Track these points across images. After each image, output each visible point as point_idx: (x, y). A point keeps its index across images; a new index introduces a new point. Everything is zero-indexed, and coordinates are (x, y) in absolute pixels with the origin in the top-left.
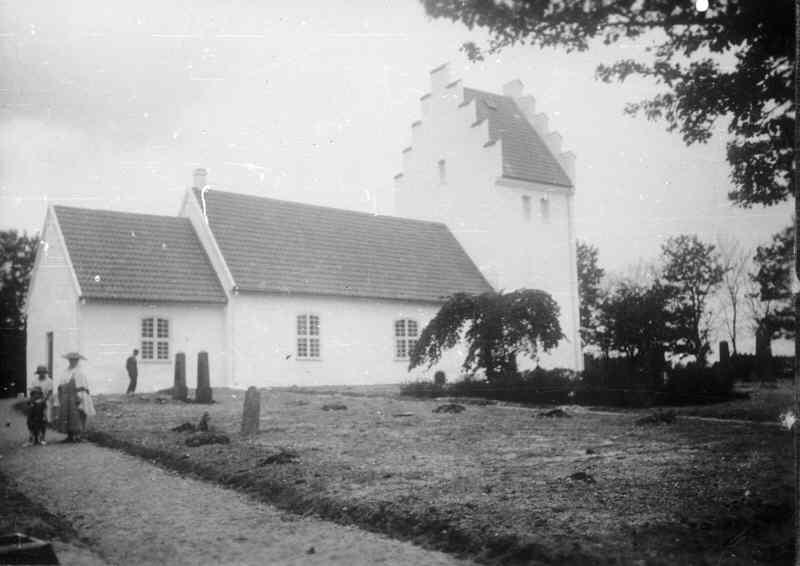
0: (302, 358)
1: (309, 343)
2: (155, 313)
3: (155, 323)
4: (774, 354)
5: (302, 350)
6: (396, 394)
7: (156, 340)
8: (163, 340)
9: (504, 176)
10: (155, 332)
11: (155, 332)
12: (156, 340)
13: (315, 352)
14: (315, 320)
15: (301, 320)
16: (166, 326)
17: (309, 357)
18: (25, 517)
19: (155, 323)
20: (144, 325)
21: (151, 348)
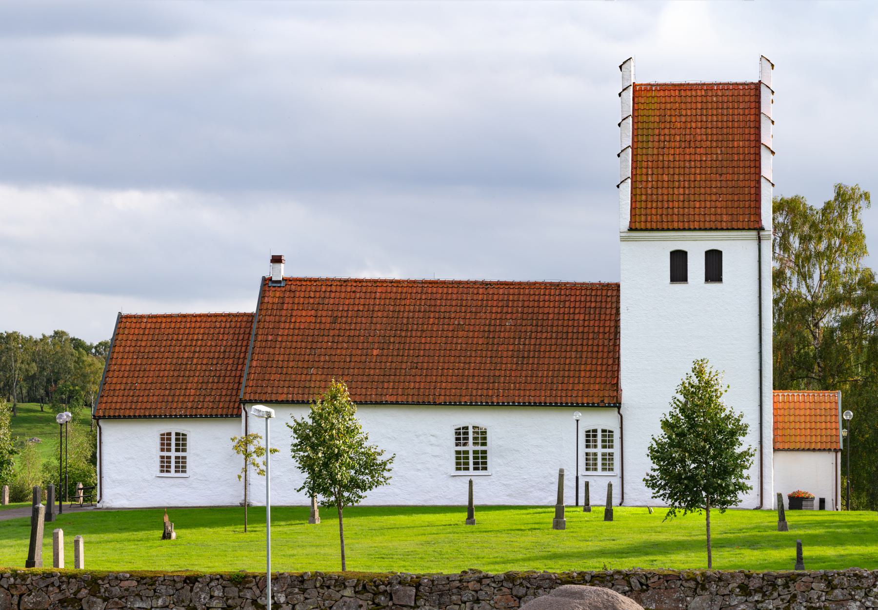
0: (165, 474)
1: (471, 456)
2: (173, 427)
3: (173, 437)
4: (255, 312)
5: (165, 465)
6: (160, 537)
7: (173, 454)
8: (180, 454)
9: (631, 229)
10: (173, 447)
11: (173, 447)
12: (173, 454)
13: (181, 465)
14: (481, 436)
15: (461, 435)
16: (184, 440)
17: (173, 473)
18: (391, 547)
19: (173, 437)
20: (162, 439)
21: (596, 459)
